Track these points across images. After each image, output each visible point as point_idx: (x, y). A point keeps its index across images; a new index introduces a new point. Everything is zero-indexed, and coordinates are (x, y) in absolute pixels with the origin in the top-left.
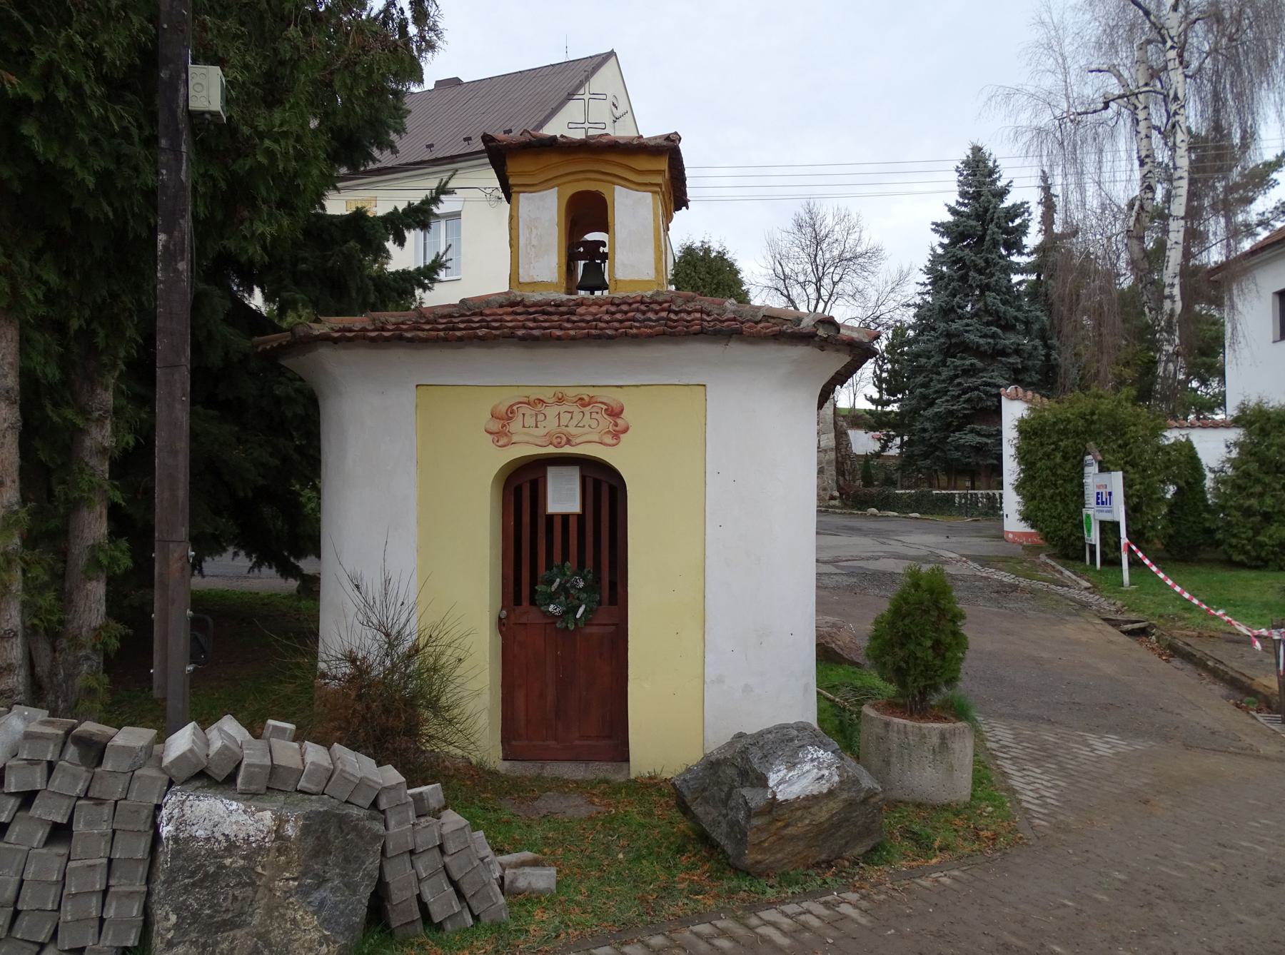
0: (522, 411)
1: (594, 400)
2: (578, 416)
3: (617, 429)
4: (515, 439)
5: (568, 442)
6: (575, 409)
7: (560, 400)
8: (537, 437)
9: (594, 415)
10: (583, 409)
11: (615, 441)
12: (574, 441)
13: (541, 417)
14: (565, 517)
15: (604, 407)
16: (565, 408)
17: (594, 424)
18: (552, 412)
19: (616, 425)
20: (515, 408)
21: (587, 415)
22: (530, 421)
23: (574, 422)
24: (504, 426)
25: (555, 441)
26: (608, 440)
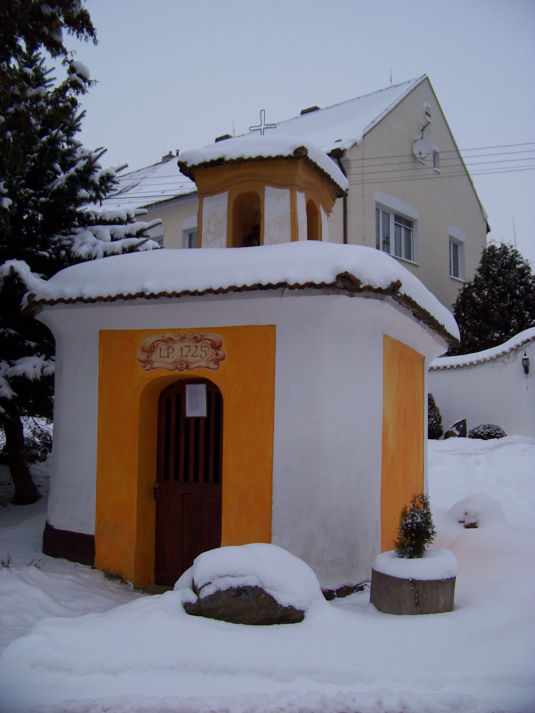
0: (159, 346)
1: (203, 338)
2: (193, 349)
4: (155, 365)
6: (192, 344)
7: (183, 339)
8: (168, 364)
9: (204, 348)
10: (197, 344)
11: (216, 366)
12: (191, 367)
13: (171, 350)
14: (197, 420)
15: (210, 342)
16: (185, 344)
17: (203, 354)
18: (177, 347)
19: (217, 355)
20: (155, 344)
21: (199, 348)
22: (164, 353)
23: (191, 353)
24: (148, 356)
25: (179, 367)
26: (212, 365)
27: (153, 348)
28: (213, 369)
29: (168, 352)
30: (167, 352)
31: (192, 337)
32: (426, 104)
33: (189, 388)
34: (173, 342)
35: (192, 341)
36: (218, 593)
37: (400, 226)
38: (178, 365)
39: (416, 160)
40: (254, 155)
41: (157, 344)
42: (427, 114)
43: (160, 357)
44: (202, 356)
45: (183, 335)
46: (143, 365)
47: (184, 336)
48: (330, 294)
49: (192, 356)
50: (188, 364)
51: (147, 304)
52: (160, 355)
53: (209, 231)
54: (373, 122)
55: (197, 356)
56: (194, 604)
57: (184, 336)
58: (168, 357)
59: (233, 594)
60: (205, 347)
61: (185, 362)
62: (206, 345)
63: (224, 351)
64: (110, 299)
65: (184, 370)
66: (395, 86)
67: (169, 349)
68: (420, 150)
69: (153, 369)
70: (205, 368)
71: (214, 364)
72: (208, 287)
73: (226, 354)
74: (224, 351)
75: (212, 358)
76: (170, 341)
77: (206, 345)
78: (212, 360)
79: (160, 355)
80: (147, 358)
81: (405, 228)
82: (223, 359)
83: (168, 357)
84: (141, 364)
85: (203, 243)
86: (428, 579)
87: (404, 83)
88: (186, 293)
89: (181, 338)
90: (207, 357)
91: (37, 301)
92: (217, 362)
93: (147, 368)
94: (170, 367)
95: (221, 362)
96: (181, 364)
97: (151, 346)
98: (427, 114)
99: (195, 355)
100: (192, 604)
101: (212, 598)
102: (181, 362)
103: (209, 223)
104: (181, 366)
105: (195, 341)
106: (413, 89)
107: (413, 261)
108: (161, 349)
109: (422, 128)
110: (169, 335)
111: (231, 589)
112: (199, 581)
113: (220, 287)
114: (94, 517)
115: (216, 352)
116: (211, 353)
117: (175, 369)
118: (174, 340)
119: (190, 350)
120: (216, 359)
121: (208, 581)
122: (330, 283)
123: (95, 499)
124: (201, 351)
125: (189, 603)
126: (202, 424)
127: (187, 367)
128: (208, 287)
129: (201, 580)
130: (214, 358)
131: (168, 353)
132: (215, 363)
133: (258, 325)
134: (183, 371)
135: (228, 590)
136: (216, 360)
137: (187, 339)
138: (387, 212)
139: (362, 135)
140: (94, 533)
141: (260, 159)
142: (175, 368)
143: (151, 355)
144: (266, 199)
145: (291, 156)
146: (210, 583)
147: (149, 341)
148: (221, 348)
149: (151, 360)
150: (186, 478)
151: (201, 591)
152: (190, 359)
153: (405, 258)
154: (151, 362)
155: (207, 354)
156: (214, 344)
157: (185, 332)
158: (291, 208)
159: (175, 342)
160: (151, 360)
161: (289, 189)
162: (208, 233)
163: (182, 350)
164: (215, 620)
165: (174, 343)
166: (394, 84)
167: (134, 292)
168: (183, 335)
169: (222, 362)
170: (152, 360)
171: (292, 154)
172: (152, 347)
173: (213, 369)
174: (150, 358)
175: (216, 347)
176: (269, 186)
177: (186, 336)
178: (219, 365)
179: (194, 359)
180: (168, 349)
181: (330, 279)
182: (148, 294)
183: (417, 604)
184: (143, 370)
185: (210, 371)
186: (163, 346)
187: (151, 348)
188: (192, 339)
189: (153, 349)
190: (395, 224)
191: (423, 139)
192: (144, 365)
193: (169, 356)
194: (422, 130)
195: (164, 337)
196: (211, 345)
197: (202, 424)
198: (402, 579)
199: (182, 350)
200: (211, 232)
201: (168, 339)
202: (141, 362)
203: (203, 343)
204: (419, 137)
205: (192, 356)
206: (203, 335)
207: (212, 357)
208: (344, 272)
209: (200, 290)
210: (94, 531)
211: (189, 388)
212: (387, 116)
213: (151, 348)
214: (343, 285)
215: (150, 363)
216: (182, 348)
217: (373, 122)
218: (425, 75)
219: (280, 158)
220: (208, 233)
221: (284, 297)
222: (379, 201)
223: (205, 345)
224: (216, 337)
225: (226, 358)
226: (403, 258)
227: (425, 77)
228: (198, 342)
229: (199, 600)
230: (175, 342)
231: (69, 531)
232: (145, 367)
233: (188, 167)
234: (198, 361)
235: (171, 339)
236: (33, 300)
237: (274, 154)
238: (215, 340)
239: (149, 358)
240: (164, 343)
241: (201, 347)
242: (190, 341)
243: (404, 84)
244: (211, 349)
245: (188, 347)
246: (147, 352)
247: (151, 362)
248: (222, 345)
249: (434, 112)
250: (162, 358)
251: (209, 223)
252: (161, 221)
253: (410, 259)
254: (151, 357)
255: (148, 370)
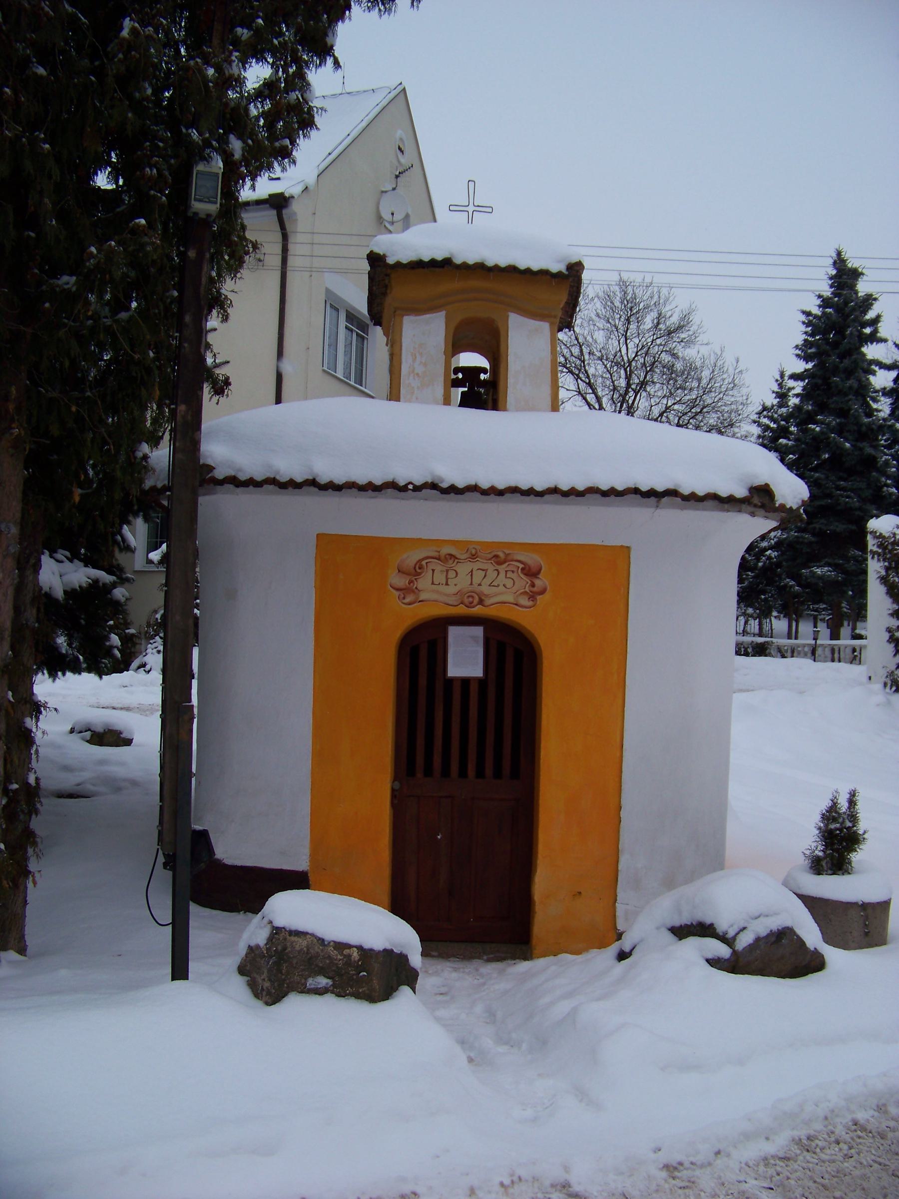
0: (431, 567)
1: (509, 558)
2: (492, 574)
3: (535, 589)
4: (423, 596)
5: (481, 602)
6: (490, 568)
7: (474, 557)
8: (448, 595)
9: (510, 574)
10: (498, 567)
11: (530, 603)
12: (488, 602)
13: (452, 574)
14: (465, 682)
15: (521, 566)
16: (479, 565)
17: (509, 583)
18: (464, 569)
19: (533, 585)
20: (424, 563)
21: (502, 574)
22: (440, 577)
23: (487, 581)
24: (411, 582)
25: (466, 601)
26: (524, 601)
27: (420, 568)
28: (526, 607)
29: (447, 576)
30: (445, 576)
31: (490, 556)
32: (399, 133)
33: (454, 632)
34: (456, 561)
35: (490, 561)
36: (758, 940)
37: (351, 331)
38: (465, 598)
39: (381, 223)
40: (503, 263)
41: (427, 563)
42: (400, 149)
43: (433, 583)
44: (508, 587)
45: (474, 552)
46: (400, 595)
47: (476, 553)
48: (728, 511)
49: (489, 586)
50: (483, 598)
51: (426, 500)
52: (433, 581)
53: (413, 371)
54: (330, 154)
55: (498, 586)
56: (728, 960)
57: (476, 553)
58: (447, 584)
59: (773, 939)
60: (513, 572)
61: (478, 595)
62: (515, 570)
63: (545, 580)
64: (371, 488)
65: (477, 605)
66: (349, 93)
67: (449, 573)
68: (393, 209)
69: (420, 603)
70: (512, 605)
71: (527, 599)
72: (552, 485)
73: (547, 584)
74: (545, 580)
75: (523, 590)
76: (451, 559)
77: (515, 570)
78: (525, 593)
79: (433, 581)
80: (407, 584)
81: (358, 334)
82: (543, 592)
83: (447, 584)
84: (396, 593)
85: (403, 391)
86: (878, 901)
87: (365, 91)
88: (514, 490)
89: (470, 556)
90: (514, 590)
91: (241, 479)
92: (532, 596)
93: (407, 600)
94: (451, 600)
95: (539, 597)
96: (469, 597)
97: (416, 565)
98: (400, 149)
99: (495, 583)
100: (723, 960)
101: (752, 947)
102: (470, 594)
103: (414, 360)
104: (471, 599)
105: (494, 562)
106: (386, 104)
107: (366, 388)
108: (433, 570)
109: (397, 173)
110: (446, 550)
111: (771, 933)
112: (729, 927)
113: (571, 486)
114: (307, 842)
115: (531, 581)
116: (522, 582)
117: (459, 604)
118: (457, 558)
119: (485, 576)
120: (531, 592)
121: (742, 925)
122: (742, 497)
123: (307, 810)
124: (506, 578)
125: (716, 958)
126: (474, 689)
127: (481, 602)
128: (551, 485)
129: (732, 926)
130: (527, 590)
131: (447, 579)
132: (529, 598)
133: (603, 544)
134: (473, 607)
135: (768, 936)
136: (531, 593)
137: (482, 559)
138: (336, 306)
139: (316, 173)
140: (308, 868)
141: (512, 270)
142: (459, 602)
143: (415, 579)
144: (511, 333)
145: (564, 273)
146: (744, 928)
147: (412, 557)
148: (540, 576)
149: (416, 588)
150: (446, 773)
151: (738, 941)
152: (485, 589)
153: (355, 383)
154: (416, 590)
155: (516, 584)
156: (527, 568)
157: (478, 547)
158: (551, 353)
159: (460, 561)
160: (416, 588)
161: (547, 322)
162: (412, 375)
163: (472, 575)
164: (812, 975)
165: (458, 562)
166: (348, 91)
167: (419, 480)
168: (474, 552)
169: (541, 596)
170: (418, 588)
171: (564, 271)
172: (417, 568)
173: (526, 607)
174: (414, 585)
175: (531, 573)
176: (514, 313)
177: (479, 554)
178: (537, 601)
179: (494, 590)
180: (447, 571)
181: (741, 492)
182: (445, 485)
183: (867, 934)
184: (400, 603)
185: (521, 609)
186: (438, 567)
187: (415, 568)
188: (490, 559)
189: (419, 571)
190: (347, 327)
191: (396, 191)
192: (403, 596)
193: (449, 583)
194: (397, 177)
195: (439, 552)
196: (523, 569)
197: (474, 689)
198: (848, 903)
199: (472, 575)
200: (418, 374)
201: (447, 556)
202: (398, 590)
203: (508, 565)
204: (389, 187)
205: (489, 586)
206: (509, 554)
207: (525, 588)
208: (763, 484)
209: (539, 488)
210: (308, 864)
211: (454, 632)
212: (352, 144)
213: (415, 568)
214: (761, 502)
215: (413, 592)
216: (472, 571)
217: (330, 154)
218: (401, 84)
219: (544, 273)
220: (412, 375)
221: (660, 508)
222: (331, 288)
223: (513, 569)
224: (532, 559)
225: (547, 591)
226: (352, 383)
227: (400, 88)
228: (500, 563)
229: (735, 952)
230: (460, 561)
231: (255, 867)
232: (404, 598)
233: (389, 264)
234: (502, 593)
235: (451, 556)
236: (211, 477)
237: (535, 266)
238: (529, 562)
239: (412, 584)
240: (440, 562)
241: (506, 571)
242: (485, 561)
243: (366, 93)
244: (522, 576)
245: (483, 570)
246: (408, 574)
247: (416, 590)
248: (542, 571)
249: (408, 148)
250: (436, 586)
251: (414, 360)
252: (217, 327)
253: (361, 386)
254: (415, 582)
255: (410, 604)
